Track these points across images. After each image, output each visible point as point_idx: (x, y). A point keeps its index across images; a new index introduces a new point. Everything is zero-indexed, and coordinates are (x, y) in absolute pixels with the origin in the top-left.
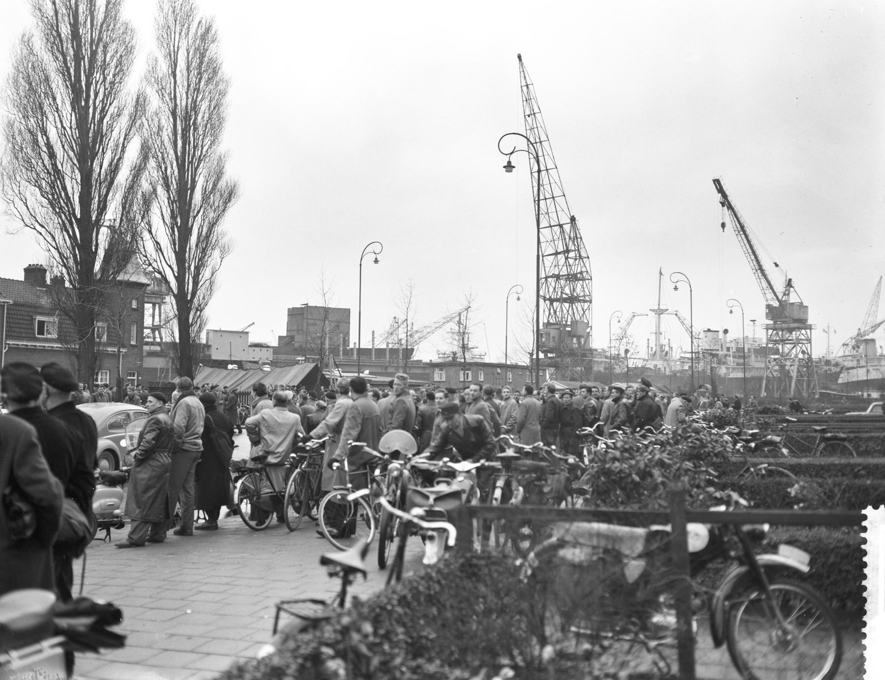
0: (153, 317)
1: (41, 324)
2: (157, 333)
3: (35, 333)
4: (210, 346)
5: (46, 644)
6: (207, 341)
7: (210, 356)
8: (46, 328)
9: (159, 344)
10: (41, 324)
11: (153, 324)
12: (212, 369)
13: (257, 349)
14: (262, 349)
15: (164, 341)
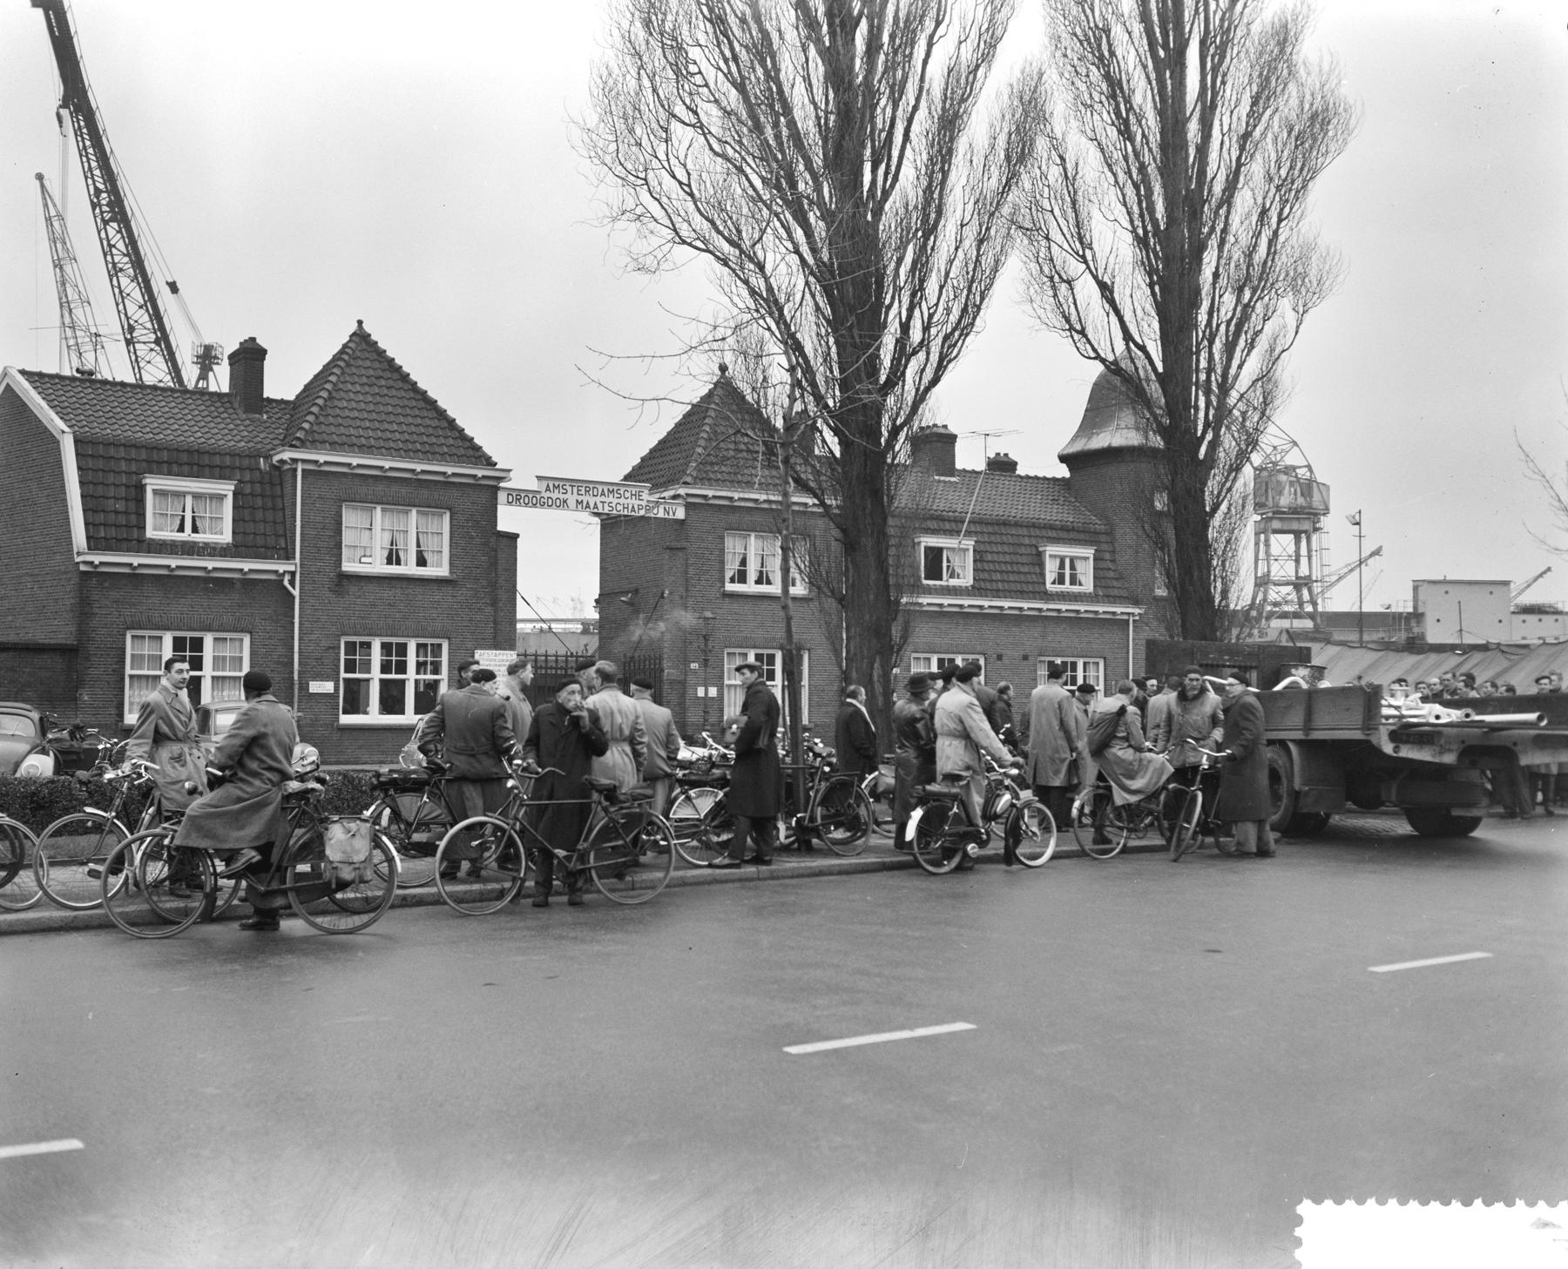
0: (1297, 561)
1: (935, 555)
2: (1305, 592)
3: (919, 577)
4: (1422, 615)
5: (467, 794)
6: (1415, 607)
7: (1422, 636)
8: (945, 564)
9: (1312, 616)
10: (935, 555)
11: (1297, 578)
12: (1421, 657)
13: (1532, 619)
14: (1544, 617)
15: (1320, 609)
